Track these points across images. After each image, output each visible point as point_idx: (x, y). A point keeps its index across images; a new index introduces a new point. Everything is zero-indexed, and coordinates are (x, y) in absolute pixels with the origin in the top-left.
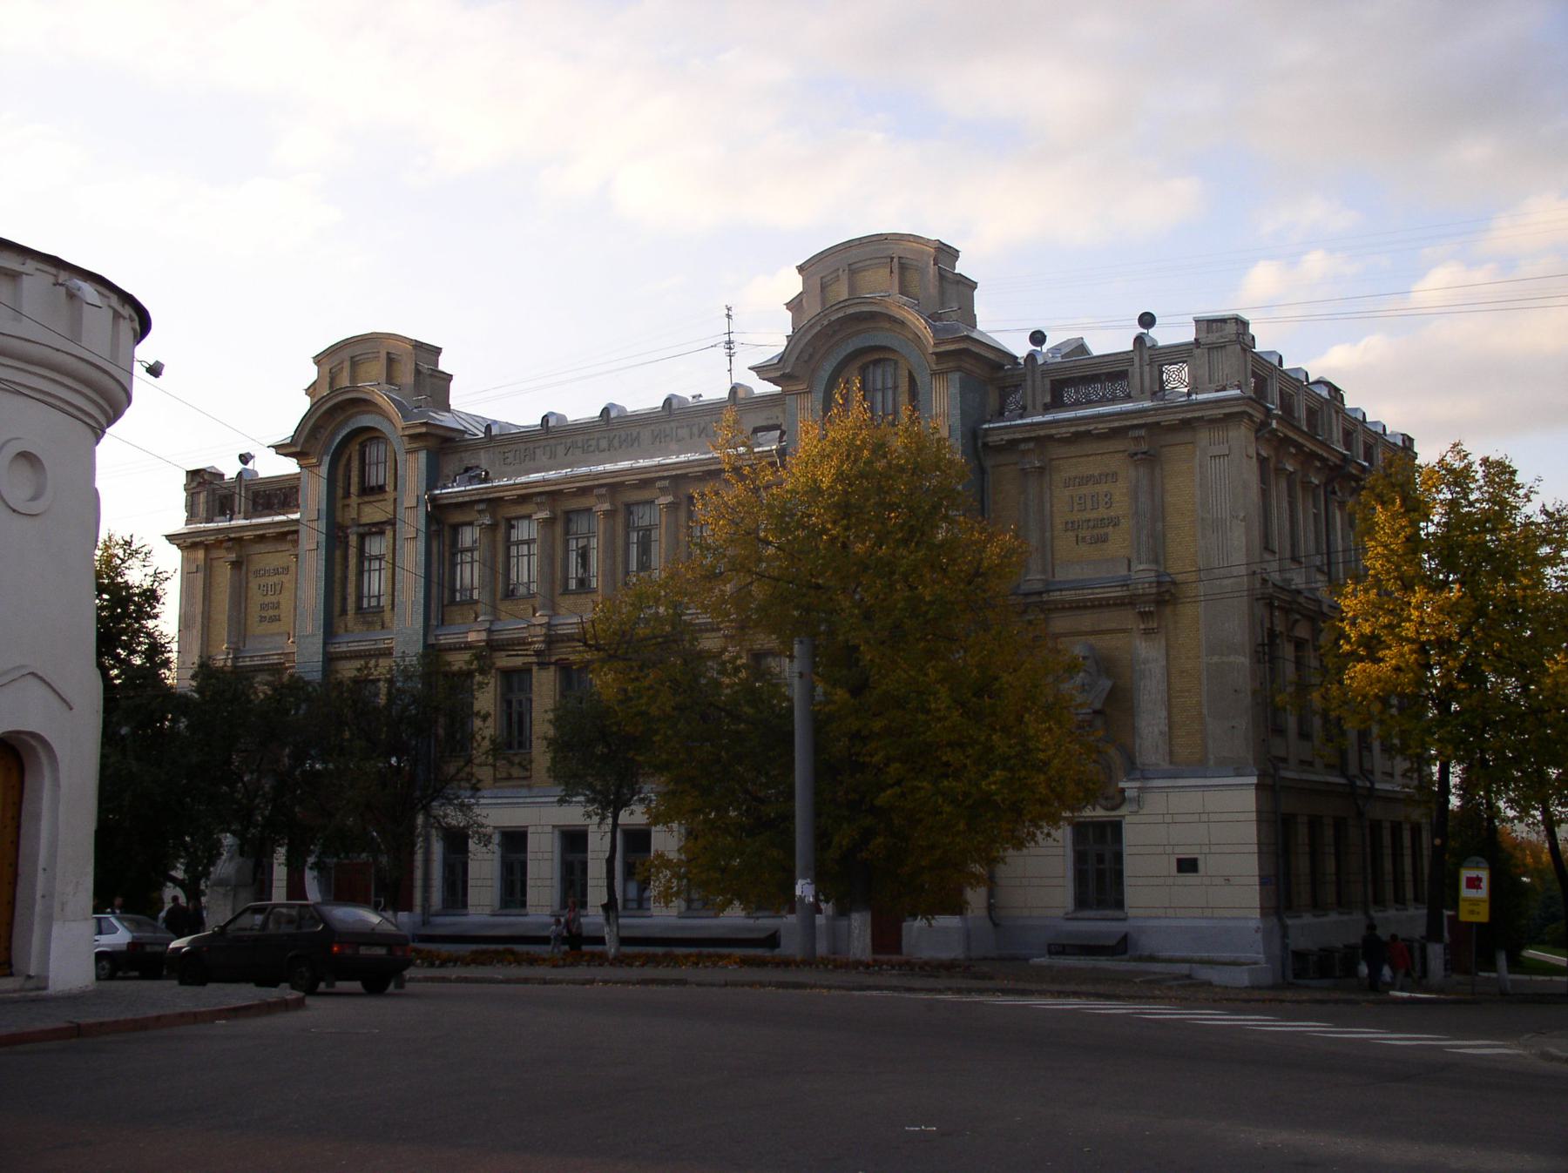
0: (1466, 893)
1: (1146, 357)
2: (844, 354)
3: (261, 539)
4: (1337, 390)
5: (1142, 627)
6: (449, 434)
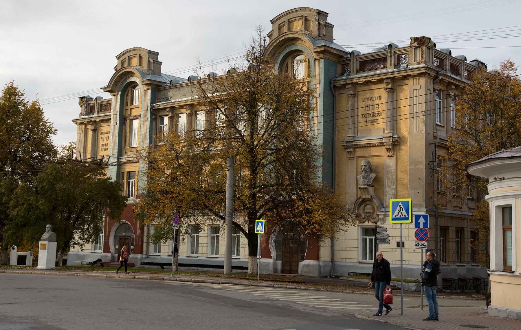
2: (286, 53)
5: (388, 154)
6: (159, 84)
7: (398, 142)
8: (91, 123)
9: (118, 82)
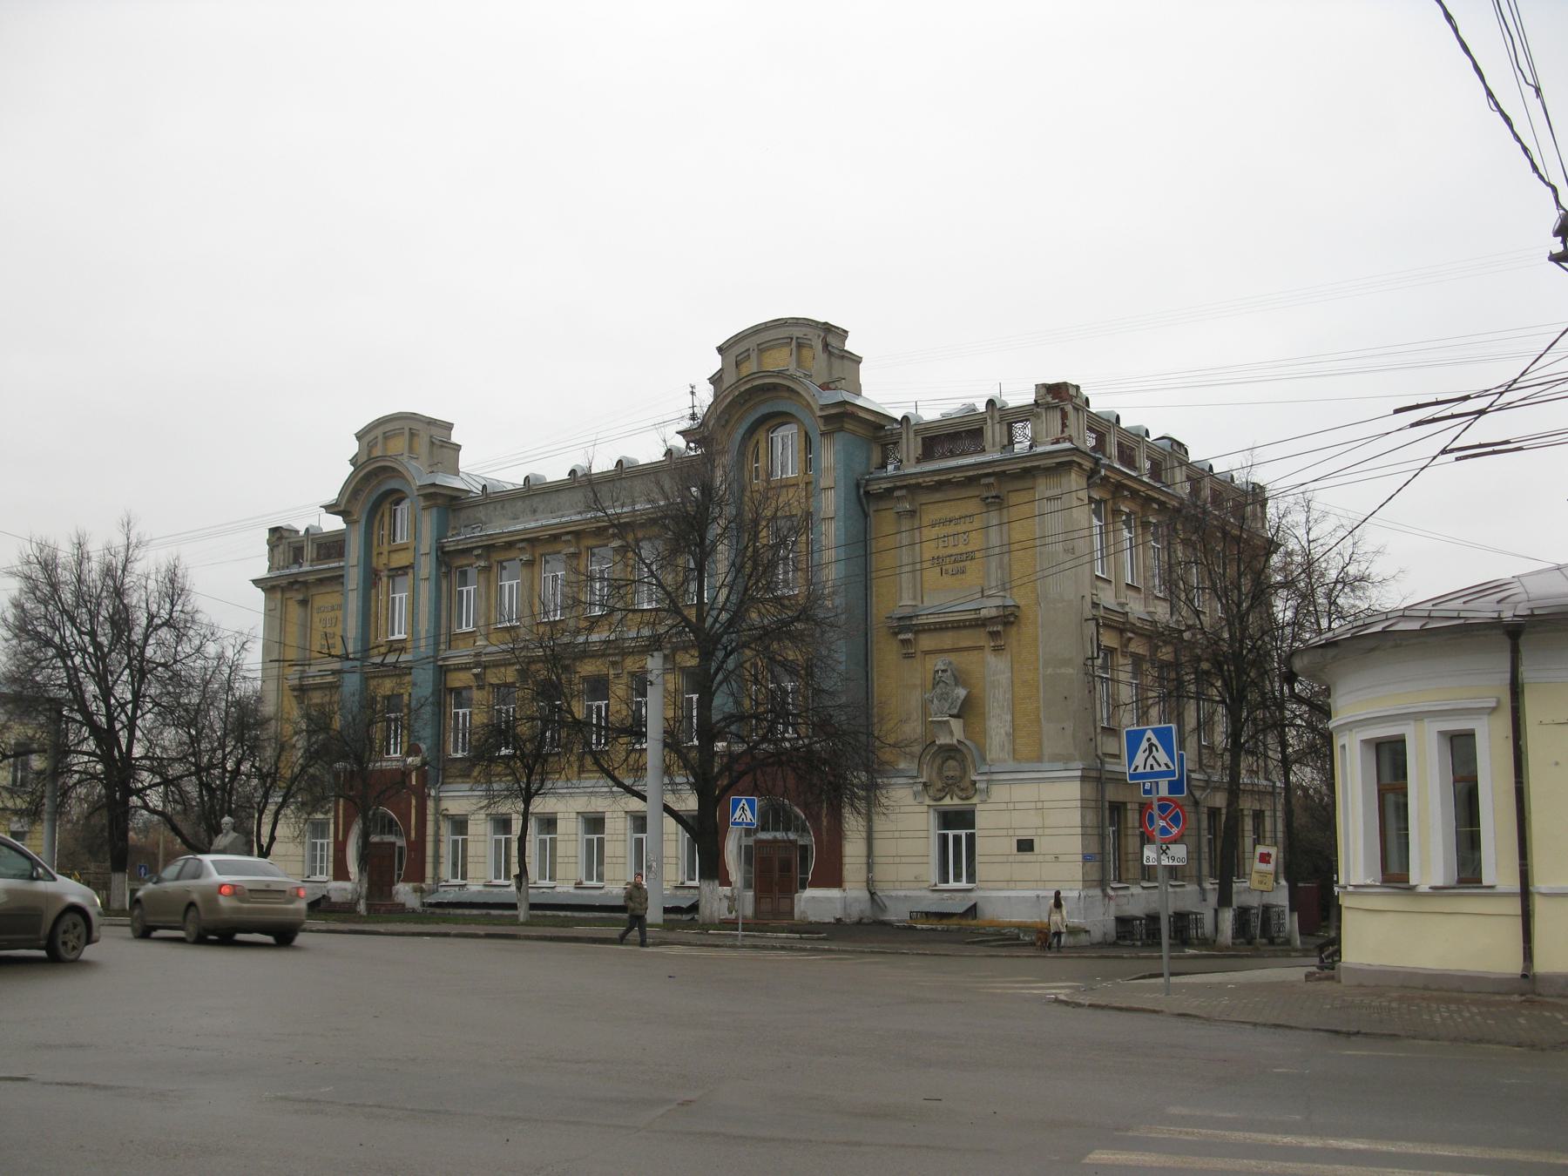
4: (1180, 445)
5: (992, 644)
7: (1016, 617)
8: (296, 587)
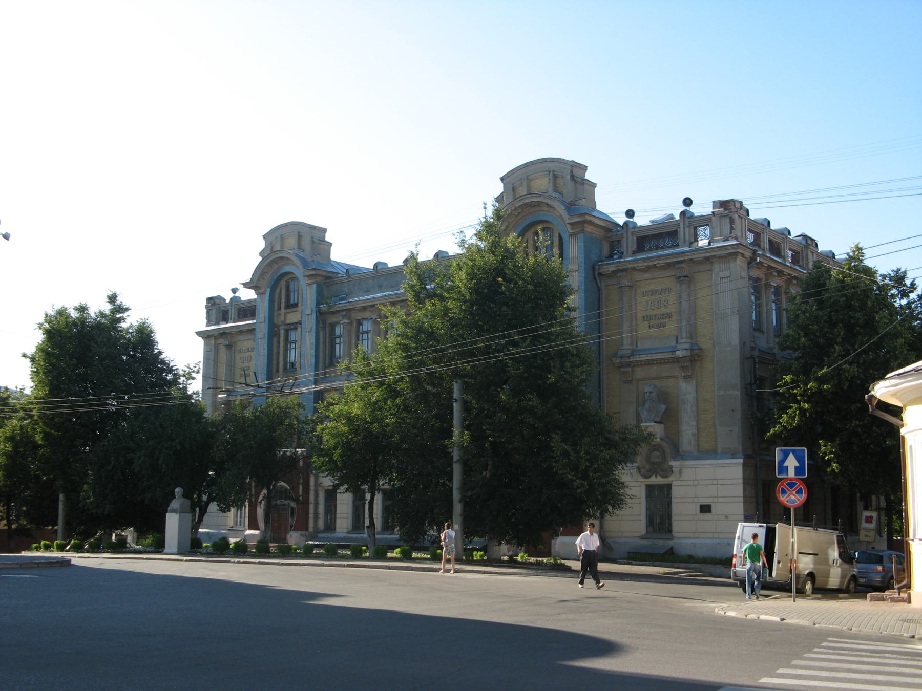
0: (864, 525)
1: (687, 223)
3: (241, 332)
5: (683, 375)
6: (329, 275)
9: (267, 273)
